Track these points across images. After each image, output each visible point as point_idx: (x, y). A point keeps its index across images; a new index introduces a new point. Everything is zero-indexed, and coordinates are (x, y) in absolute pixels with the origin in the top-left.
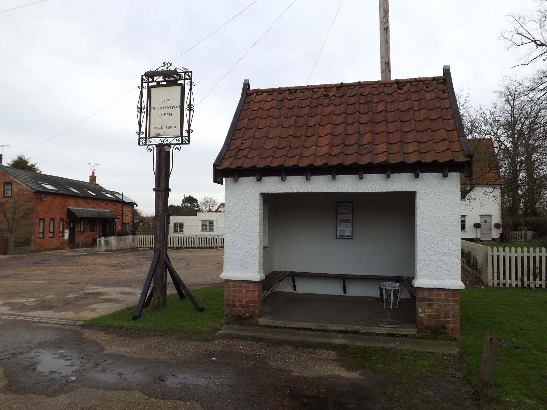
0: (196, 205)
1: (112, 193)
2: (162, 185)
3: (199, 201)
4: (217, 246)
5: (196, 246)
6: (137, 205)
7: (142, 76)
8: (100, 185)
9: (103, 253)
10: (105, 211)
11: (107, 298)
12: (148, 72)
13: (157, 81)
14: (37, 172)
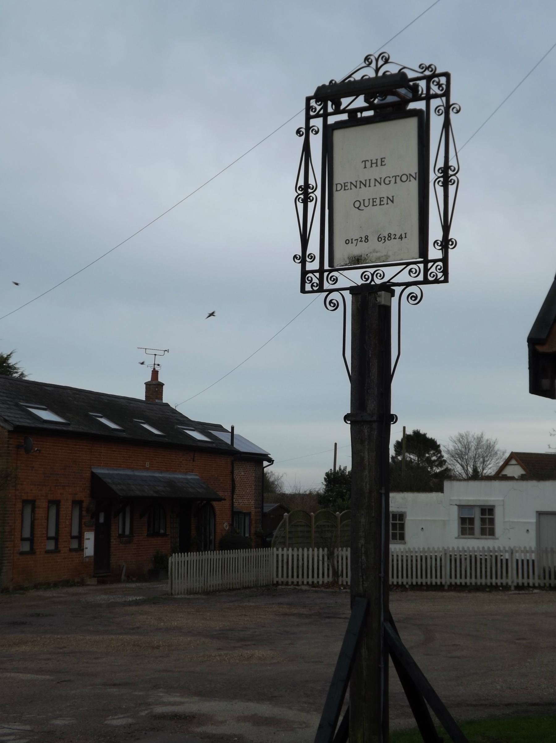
0: (434, 458)
1: (203, 427)
2: (372, 405)
3: (444, 446)
4: (510, 583)
5: (443, 583)
6: (271, 461)
7: (308, 99)
8: (172, 406)
9: (183, 596)
10: (187, 479)
11: (214, 732)
12: (324, 86)
13: (348, 108)
14: (15, 375)
